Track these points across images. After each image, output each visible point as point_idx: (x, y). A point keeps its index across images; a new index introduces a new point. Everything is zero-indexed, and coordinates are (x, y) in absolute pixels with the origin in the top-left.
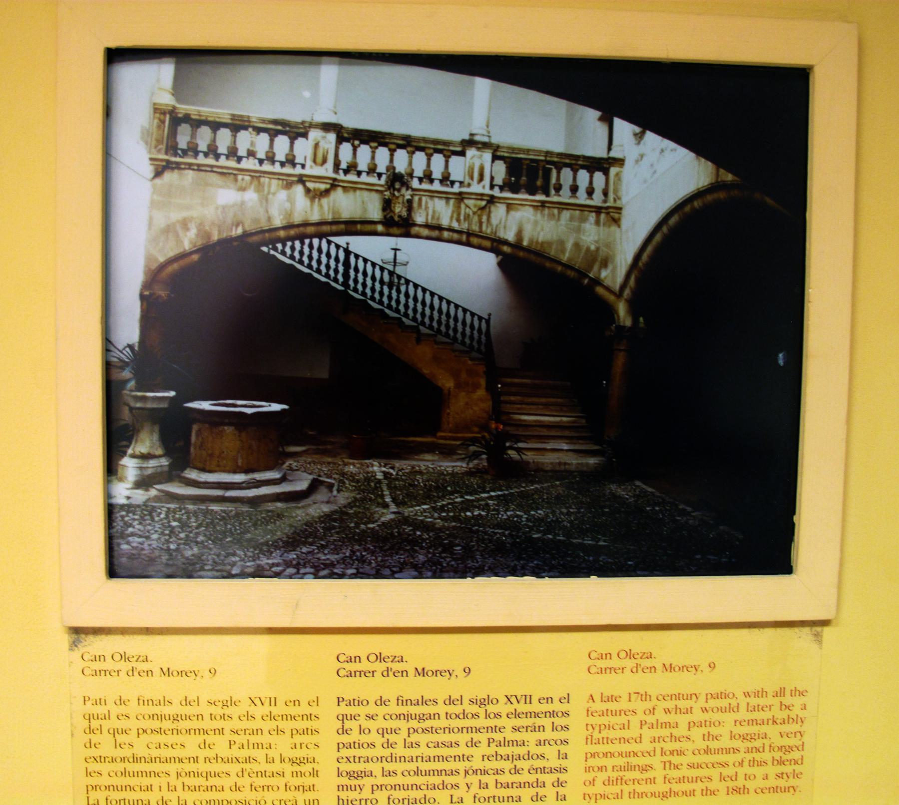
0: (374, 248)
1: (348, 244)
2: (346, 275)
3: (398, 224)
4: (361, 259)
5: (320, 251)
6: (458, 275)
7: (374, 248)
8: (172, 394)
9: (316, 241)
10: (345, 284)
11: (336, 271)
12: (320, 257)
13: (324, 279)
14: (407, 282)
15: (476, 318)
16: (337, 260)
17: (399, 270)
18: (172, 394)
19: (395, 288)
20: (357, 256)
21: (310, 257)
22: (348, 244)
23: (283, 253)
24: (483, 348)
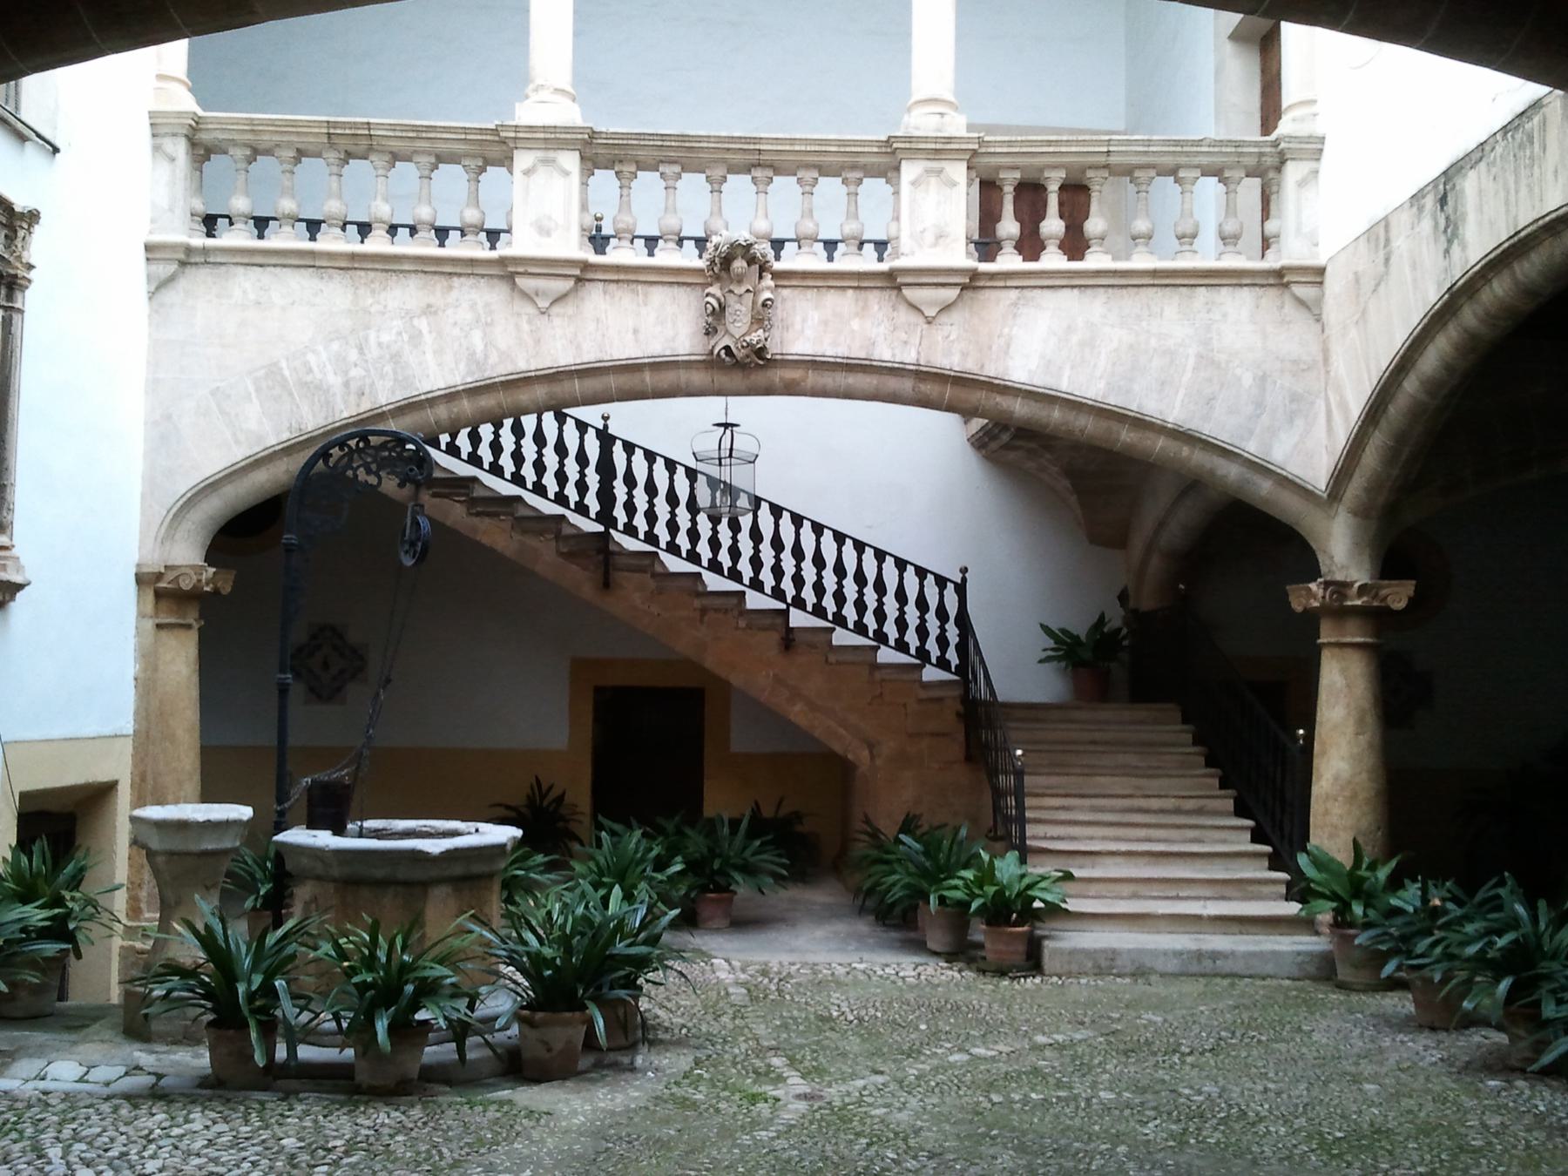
0: (672, 428)
1: (605, 418)
2: (606, 495)
3: (747, 369)
4: (930, 578)
5: (540, 439)
7: (672, 428)
8: (245, 812)
9: (529, 422)
10: (606, 517)
11: (582, 487)
14: (757, 502)
16: (582, 459)
17: (738, 476)
18: (245, 812)
19: (725, 521)
20: (629, 448)
21: (561, 477)
22: (605, 418)
23: (453, 450)
24: (952, 656)
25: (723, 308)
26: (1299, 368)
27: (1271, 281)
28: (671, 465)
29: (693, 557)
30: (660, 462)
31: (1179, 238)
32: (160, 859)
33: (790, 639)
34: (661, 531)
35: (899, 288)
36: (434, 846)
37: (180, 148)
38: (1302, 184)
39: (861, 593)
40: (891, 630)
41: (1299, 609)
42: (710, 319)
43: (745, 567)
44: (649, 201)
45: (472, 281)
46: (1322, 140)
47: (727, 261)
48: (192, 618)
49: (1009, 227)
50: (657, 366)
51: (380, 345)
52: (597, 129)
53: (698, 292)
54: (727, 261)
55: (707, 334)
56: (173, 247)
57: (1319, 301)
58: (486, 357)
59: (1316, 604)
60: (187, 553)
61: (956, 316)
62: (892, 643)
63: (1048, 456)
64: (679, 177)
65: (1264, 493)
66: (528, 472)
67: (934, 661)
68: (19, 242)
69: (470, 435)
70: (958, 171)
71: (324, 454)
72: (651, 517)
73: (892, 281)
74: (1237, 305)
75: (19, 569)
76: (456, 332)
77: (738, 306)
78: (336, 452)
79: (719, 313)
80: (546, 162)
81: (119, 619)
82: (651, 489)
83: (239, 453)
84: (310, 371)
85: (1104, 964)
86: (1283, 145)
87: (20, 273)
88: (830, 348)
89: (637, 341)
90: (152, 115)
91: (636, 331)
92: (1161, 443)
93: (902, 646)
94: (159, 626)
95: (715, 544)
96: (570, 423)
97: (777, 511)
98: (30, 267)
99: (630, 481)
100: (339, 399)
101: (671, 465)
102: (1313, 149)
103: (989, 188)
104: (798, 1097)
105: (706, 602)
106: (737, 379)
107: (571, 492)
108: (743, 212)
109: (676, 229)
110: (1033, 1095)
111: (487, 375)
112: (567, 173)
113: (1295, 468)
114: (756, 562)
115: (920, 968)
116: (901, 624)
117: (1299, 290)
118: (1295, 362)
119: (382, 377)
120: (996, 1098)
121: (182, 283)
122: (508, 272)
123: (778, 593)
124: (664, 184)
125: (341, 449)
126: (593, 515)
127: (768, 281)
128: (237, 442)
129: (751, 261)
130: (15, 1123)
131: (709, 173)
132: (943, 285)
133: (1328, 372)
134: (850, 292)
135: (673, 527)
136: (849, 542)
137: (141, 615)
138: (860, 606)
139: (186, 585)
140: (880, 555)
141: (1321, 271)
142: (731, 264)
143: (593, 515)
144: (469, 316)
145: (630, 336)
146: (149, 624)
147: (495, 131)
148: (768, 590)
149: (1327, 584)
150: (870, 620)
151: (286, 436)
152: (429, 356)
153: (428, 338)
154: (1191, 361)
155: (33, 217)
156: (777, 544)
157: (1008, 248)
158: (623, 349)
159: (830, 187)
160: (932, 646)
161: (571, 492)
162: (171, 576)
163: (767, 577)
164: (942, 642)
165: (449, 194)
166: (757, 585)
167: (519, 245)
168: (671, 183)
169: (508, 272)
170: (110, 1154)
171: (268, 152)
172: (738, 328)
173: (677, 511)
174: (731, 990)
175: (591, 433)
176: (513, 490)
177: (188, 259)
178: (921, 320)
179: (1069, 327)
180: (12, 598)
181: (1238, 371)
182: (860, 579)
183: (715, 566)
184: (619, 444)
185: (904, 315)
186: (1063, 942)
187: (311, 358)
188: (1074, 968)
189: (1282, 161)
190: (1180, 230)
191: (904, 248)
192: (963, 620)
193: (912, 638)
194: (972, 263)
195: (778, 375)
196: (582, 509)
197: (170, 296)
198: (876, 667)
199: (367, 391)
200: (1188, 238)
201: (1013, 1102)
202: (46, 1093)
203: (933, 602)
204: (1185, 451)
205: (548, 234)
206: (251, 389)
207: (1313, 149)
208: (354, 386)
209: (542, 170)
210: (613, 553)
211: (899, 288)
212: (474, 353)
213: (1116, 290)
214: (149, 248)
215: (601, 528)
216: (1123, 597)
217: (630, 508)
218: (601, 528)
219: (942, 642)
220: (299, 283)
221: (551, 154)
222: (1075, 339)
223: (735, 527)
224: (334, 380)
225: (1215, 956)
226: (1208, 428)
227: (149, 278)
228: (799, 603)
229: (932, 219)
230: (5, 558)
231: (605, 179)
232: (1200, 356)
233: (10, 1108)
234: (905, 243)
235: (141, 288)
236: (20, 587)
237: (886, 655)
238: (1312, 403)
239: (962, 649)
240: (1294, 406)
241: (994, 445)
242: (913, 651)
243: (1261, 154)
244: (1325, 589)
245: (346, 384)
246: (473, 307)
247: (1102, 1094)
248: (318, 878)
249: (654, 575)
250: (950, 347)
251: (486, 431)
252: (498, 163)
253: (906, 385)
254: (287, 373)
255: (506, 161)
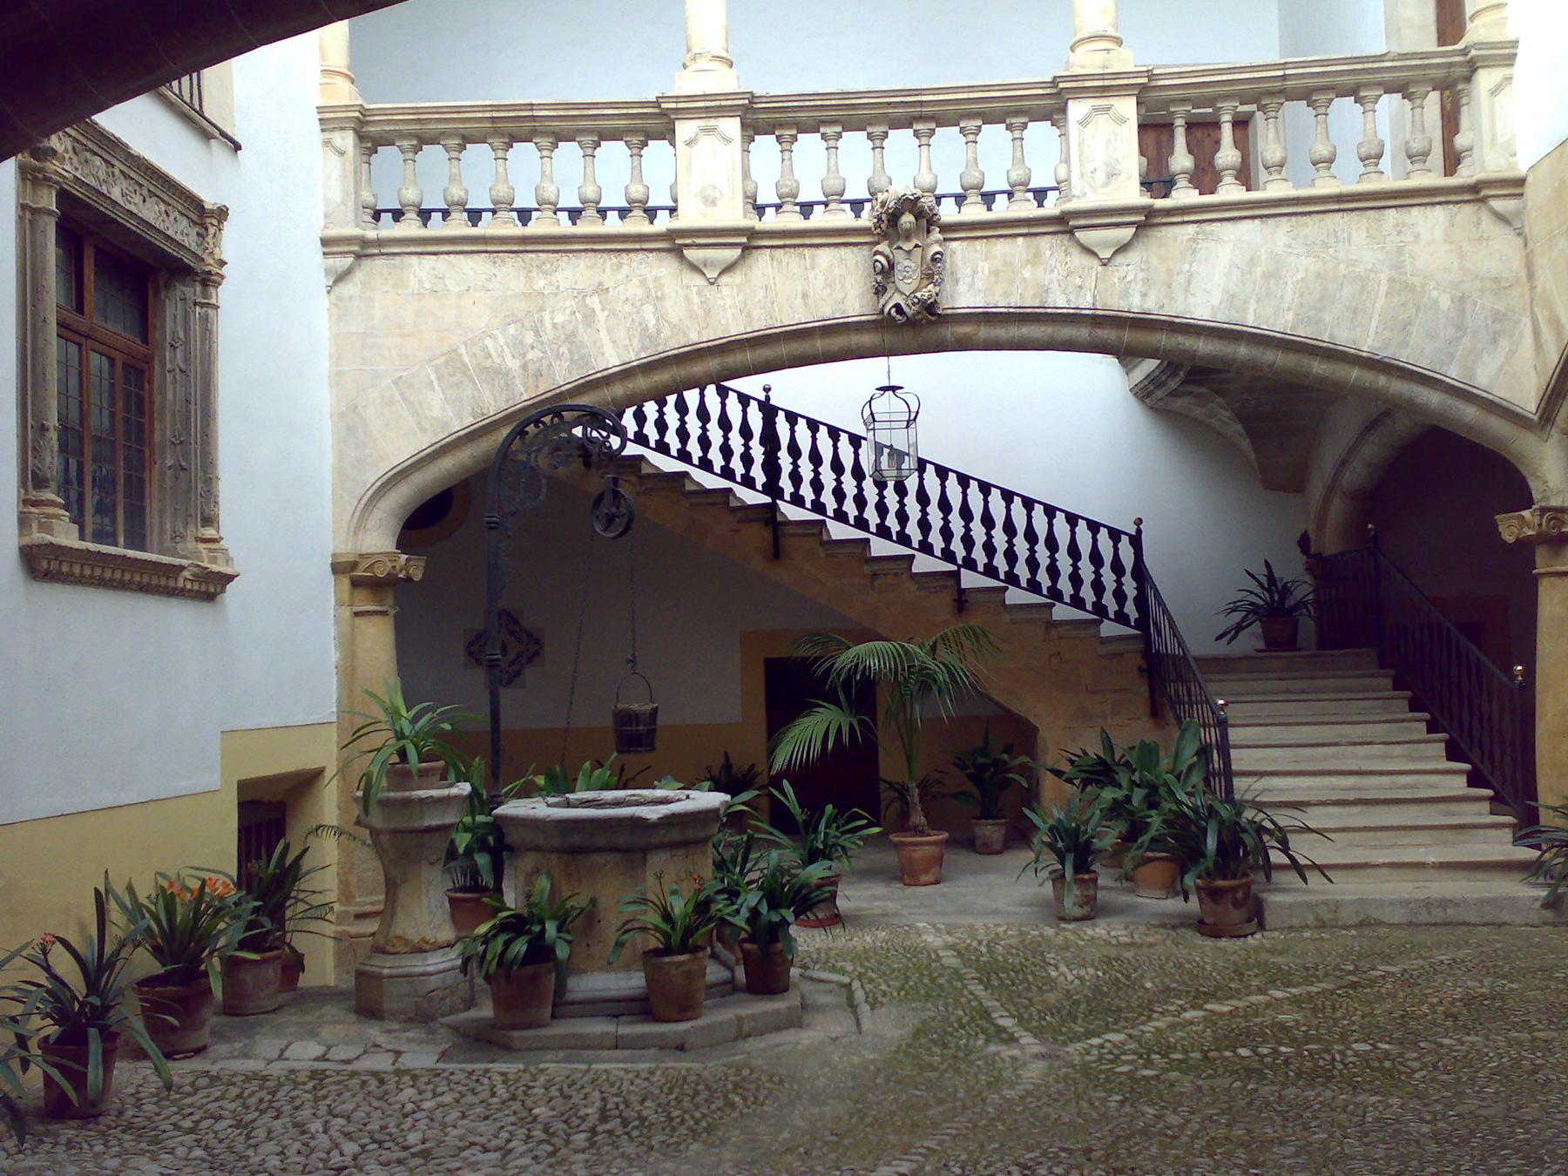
1: (767, 390)
2: (771, 467)
3: (920, 328)
4: (1103, 532)
6: (1041, 430)
9: (691, 397)
10: (772, 488)
11: (747, 460)
12: (1032, 551)
13: (669, 465)
14: (922, 464)
15: (1103, 534)
16: (746, 432)
20: (792, 418)
22: (767, 390)
24: (1130, 609)
25: (892, 266)
26: (1498, 285)
27: (1466, 197)
28: (834, 433)
29: (861, 523)
30: (823, 430)
31: (1362, 160)
32: (384, 838)
33: (962, 600)
34: (828, 499)
35: (1071, 232)
36: (653, 813)
37: (347, 140)
38: (1495, 91)
39: (1032, 551)
40: (1065, 585)
41: (1510, 539)
42: (879, 278)
43: (913, 530)
44: (812, 161)
45: (641, 255)
46: (1514, 44)
47: (894, 217)
48: (388, 605)
49: (1181, 160)
50: (828, 330)
51: (554, 325)
52: (758, 92)
53: (866, 251)
54: (894, 217)
55: (877, 293)
56: (348, 240)
57: (1519, 213)
58: (659, 332)
59: (1530, 533)
60: (379, 540)
61: (1133, 257)
62: (1067, 599)
63: (1220, 400)
64: (839, 136)
65: (1468, 419)
66: (694, 448)
67: (1112, 616)
68: (209, 239)
69: (635, 415)
70: (1128, 107)
71: (520, 432)
72: (817, 485)
73: (1064, 224)
74: (1430, 222)
75: (228, 561)
76: (628, 308)
77: (907, 263)
78: (531, 429)
79: (888, 271)
80: (707, 131)
81: (320, 608)
82: (816, 458)
83: (423, 442)
84: (490, 356)
85: (1327, 916)
86: (1473, 53)
87: (215, 270)
88: (1001, 300)
89: (806, 305)
90: (321, 110)
91: (805, 296)
92: (1355, 374)
93: (1077, 602)
94: (356, 614)
95: (882, 509)
96: (732, 397)
97: (942, 472)
98: (223, 263)
99: (794, 451)
100: (518, 381)
101: (834, 433)
102: (1505, 55)
103: (1154, 130)
104: (1036, 1056)
105: (875, 567)
106: (909, 337)
107: (737, 465)
108: (906, 164)
109: (839, 188)
110: (1283, 1049)
111: (660, 349)
112: (728, 141)
113: (1501, 391)
114: (924, 526)
115: (1132, 927)
116: (1076, 579)
117: (1497, 204)
118: (1496, 280)
119: (559, 357)
120: (1243, 1052)
121: (359, 276)
122: (675, 244)
123: (948, 555)
124: (824, 144)
125: (536, 426)
126: (759, 487)
127: (936, 235)
128: (423, 430)
129: (919, 215)
130: (270, 1101)
131: (870, 129)
132: (1117, 225)
133: (1532, 288)
134: (1021, 239)
135: (839, 494)
136: (1017, 500)
137: (339, 603)
138: (1033, 564)
139: (381, 572)
140: (1050, 511)
141: (1521, 182)
142: (904, 220)
143: (759, 487)
144: (640, 292)
145: (799, 301)
146: (346, 612)
147: (657, 104)
148: (938, 552)
149: (1543, 510)
150: (1043, 578)
151: (471, 420)
152: (603, 334)
153: (601, 316)
154: (1384, 288)
155: (222, 213)
156: (945, 506)
157: (1182, 182)
158: (794, 315)
159: (994, 134)
160: (1109, 600)
161: (737, 465)
162: (364, 564)
163: (936, 539)
164: (1120, 595)
165: (612, 170)
166: (926, 548)
167: (689, 218)
168: (832, 143)
169: (675, 244)
170: (369, 1127)
171: (434, 141)
172: (908, 287)
173: (885, 493)
174: (941, 953)
175: (754, 405)
176: (680, 467)
177: (364, 250)
178: (1096, 262)
179: (1252, 260)
180: (223, 591)
181: (1435, 294)
182: (1031, 536)
183: (883, 531)
184: (781, 414)
185: (1078, 259)
186: (1283, 896)
187: (489, 343)
188: (1296, 922)
189: (1472, 67)
190: (1364, 151)
191: (1075, 192)
192: (1140, 572)
193: (1087, 593)
194: (1146, 200)
195: (948, 332)
196: (748, 482)
197: (347, 289)
198: (1052, 625)
199: (545, 372)
200: (1371, 158)
201: (1263, 1056)
202: (292, 1071)
203: (715, 412)
204: (1382, 380)
205: (714, 203)
206: (433, 377)
207: (1505, 55)
208: (531, 368)
209: (705, 140)
210: (781, 523)
211: (1071, 232)
212: (647, 328)
213: (1300, 218)
214: (325, 242)
215: (768, 500)
216: (1304, 543)
217: (796, 478)
218: (768, 500)
219: (1120, 595)
220: (472, 267)
221: (712, 122)
222: (1259, 271)
223: (901, 490)
224: (513, 364)
225: (1444, 903)
226: (1405, 356)
227: (327, 272)
228: (970, 564)
229: (1100, 157)
230: (215, 550)
231: (766, 144)
232: (1392, 280)
233: (261, 1087)
234: (1077, 185)
235: (324, 282)
236: (231, 578)
237: (1062, 612)
238: (1518, 322)
239: (1141, 602)
240: (1498, 326)
241: (1160, 393)
242: (1089, 607)
243: (1451, 65)
244: (1541, 516)
245: (524, 367)
246: (643, 283)
247: (1355, 1046)
248: (538, 849)
249: (823, 543)
250: (1136, 285)
251: (650, 409)
252: (660, 136)
253: (1083, 333)
254: (466, 359)
255: (667, 133)
